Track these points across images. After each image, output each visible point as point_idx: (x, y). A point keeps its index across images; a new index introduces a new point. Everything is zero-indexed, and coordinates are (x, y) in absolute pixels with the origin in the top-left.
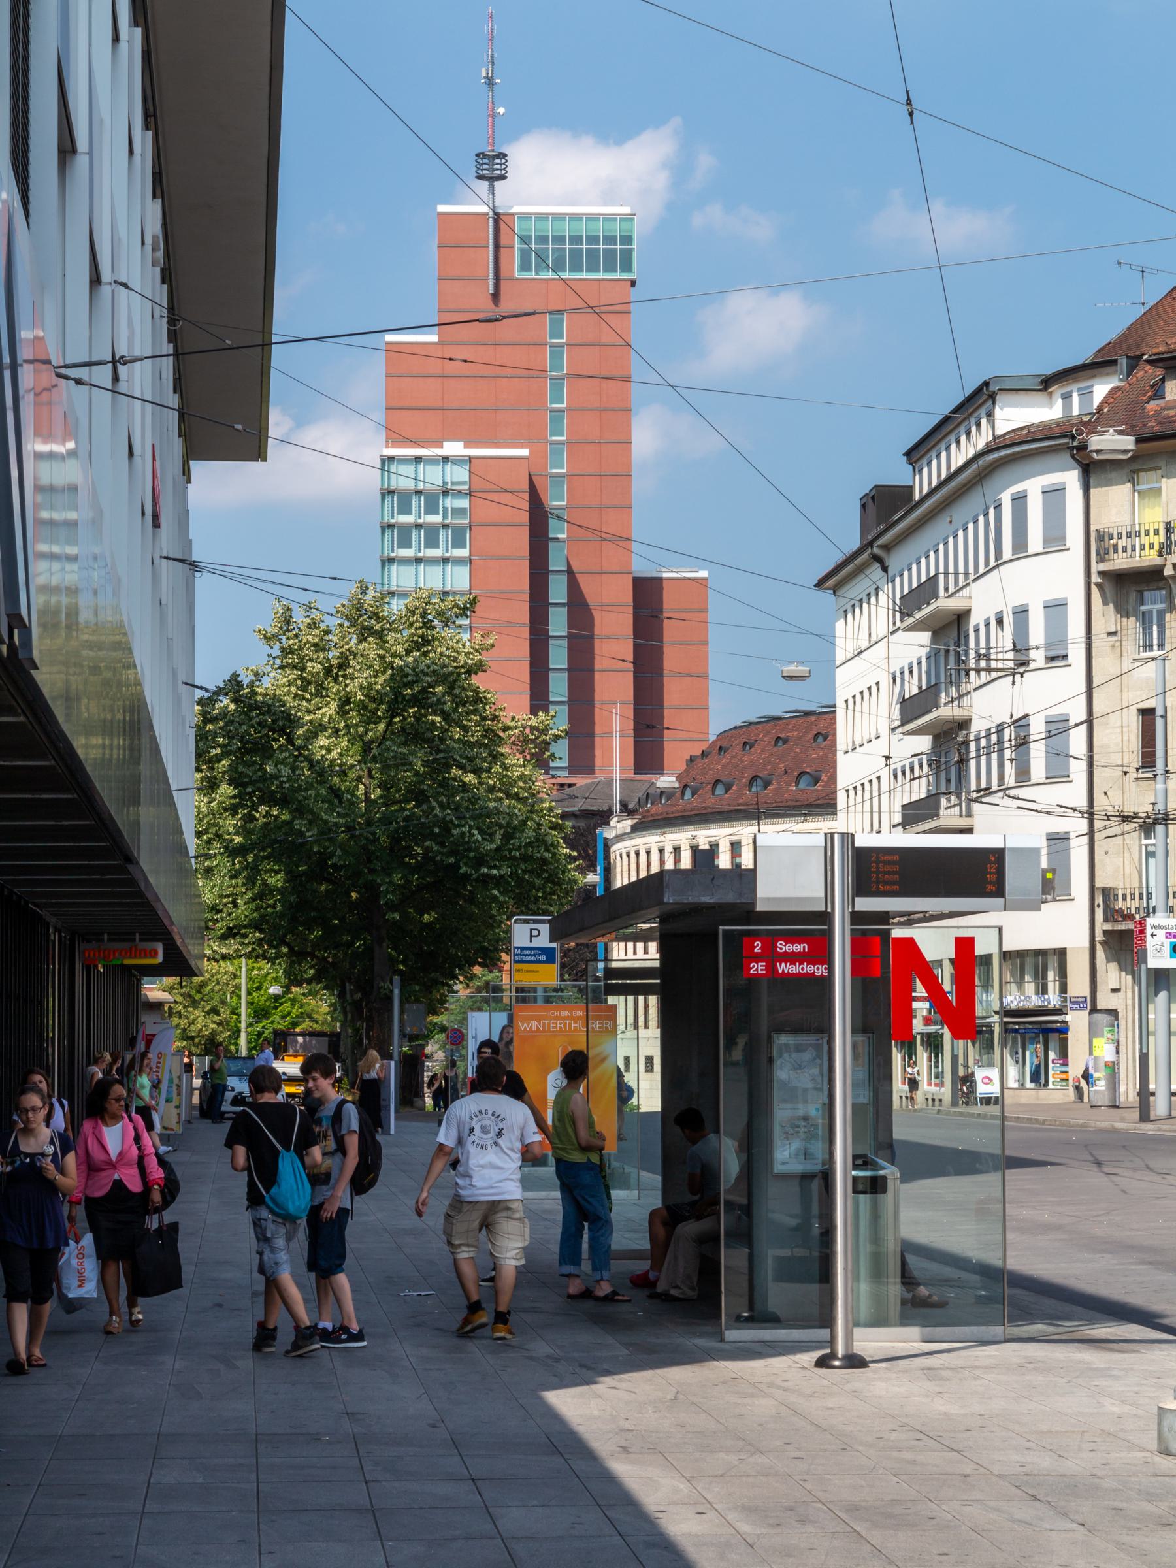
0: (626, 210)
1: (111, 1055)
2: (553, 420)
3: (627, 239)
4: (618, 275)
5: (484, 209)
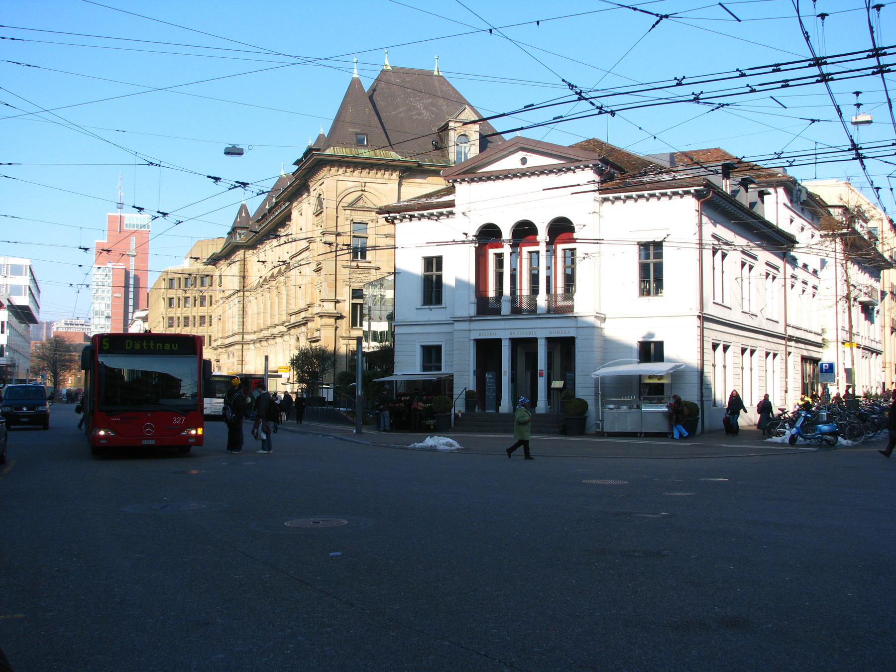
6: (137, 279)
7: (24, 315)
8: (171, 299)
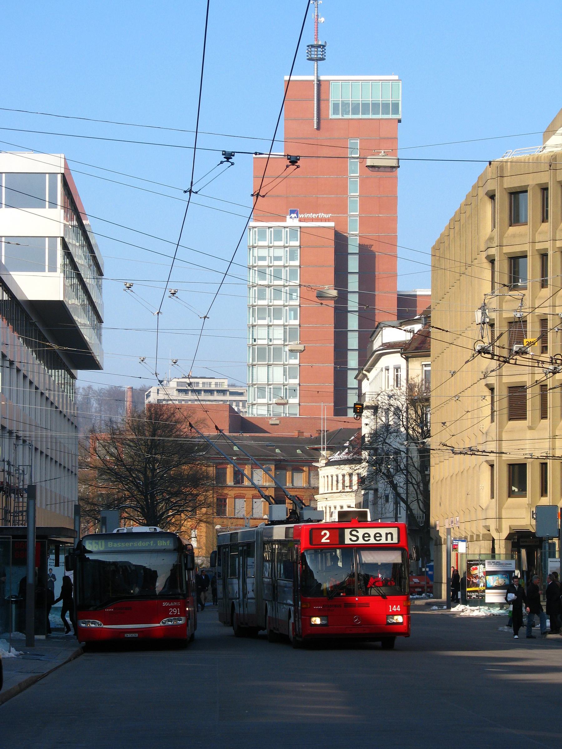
6: (367, 256)
7: (55, 334)
8: (515, 261)
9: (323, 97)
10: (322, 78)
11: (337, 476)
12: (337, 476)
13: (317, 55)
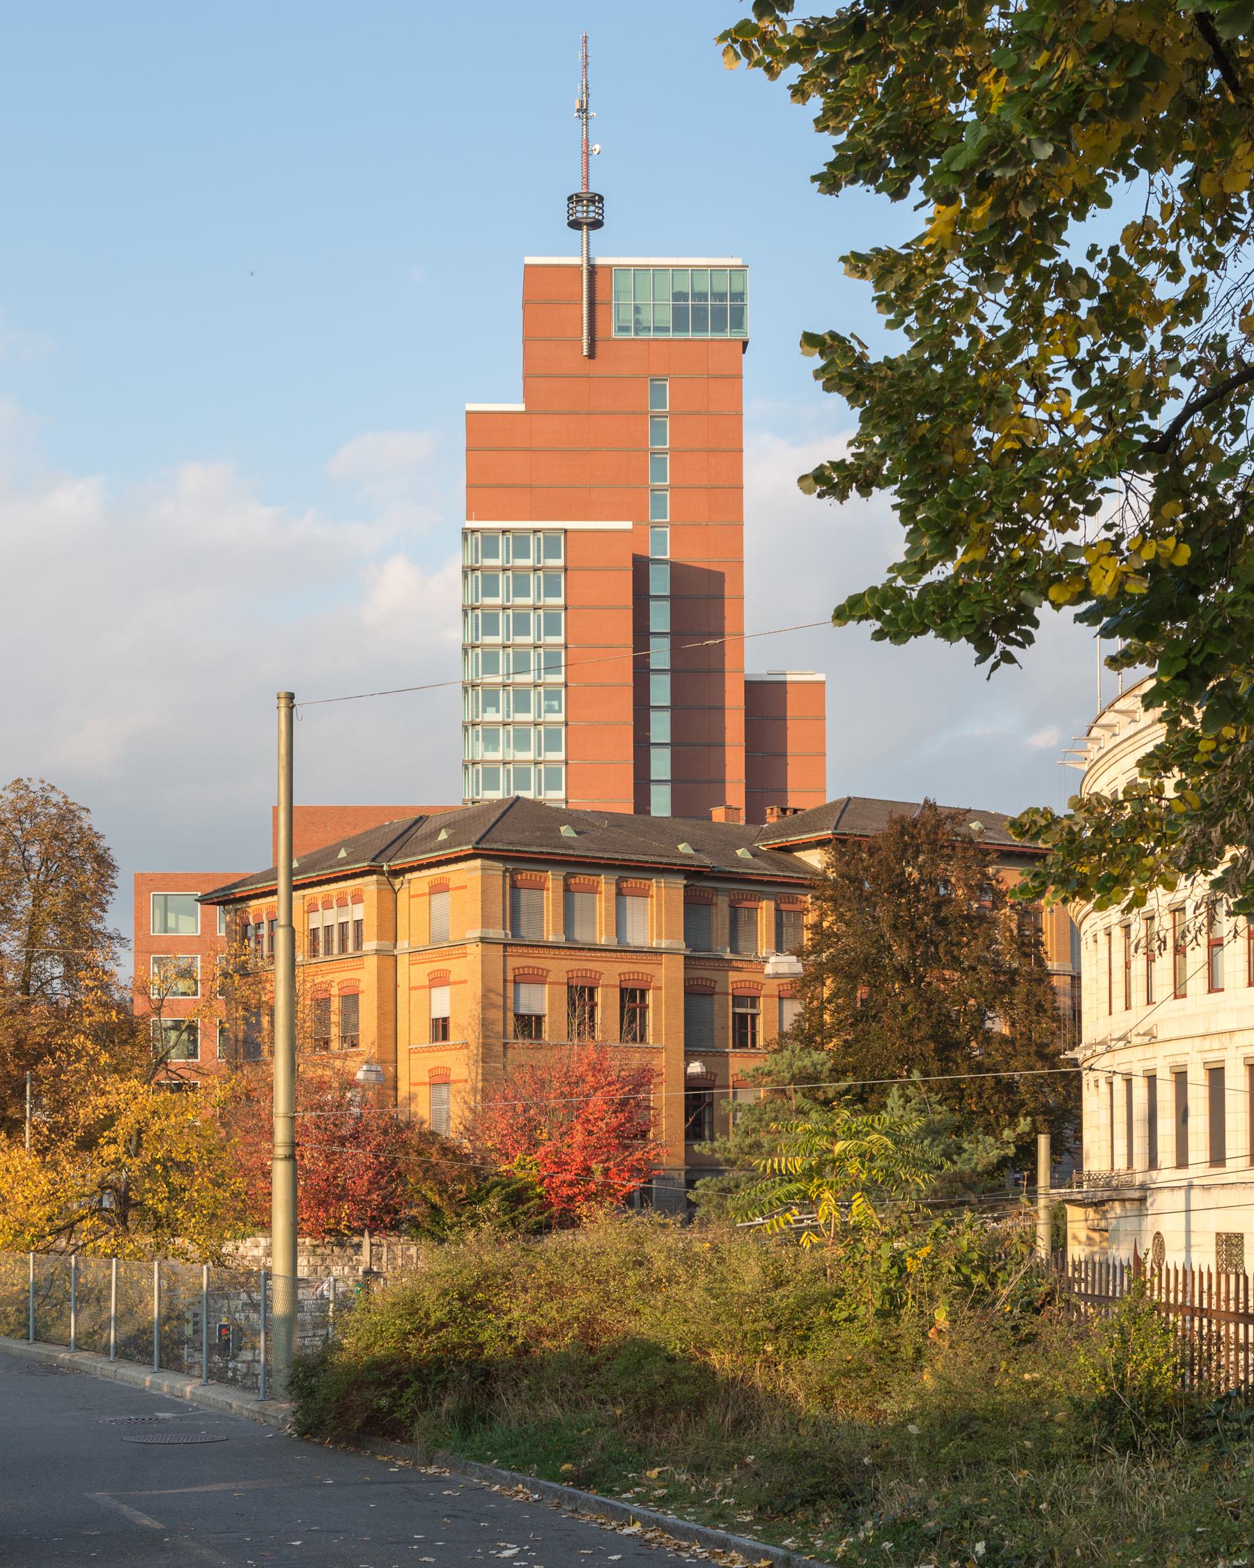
0: (737, 261)
1: (565, 1462)
2: (654, 498)
3: (740, 296)
4: (728, 335)
5: (576, 261)
9: (600, 297)
10: (599, 261)
11: (1152, 1080)
12: (1152, 1080)
13: (587, 212)
